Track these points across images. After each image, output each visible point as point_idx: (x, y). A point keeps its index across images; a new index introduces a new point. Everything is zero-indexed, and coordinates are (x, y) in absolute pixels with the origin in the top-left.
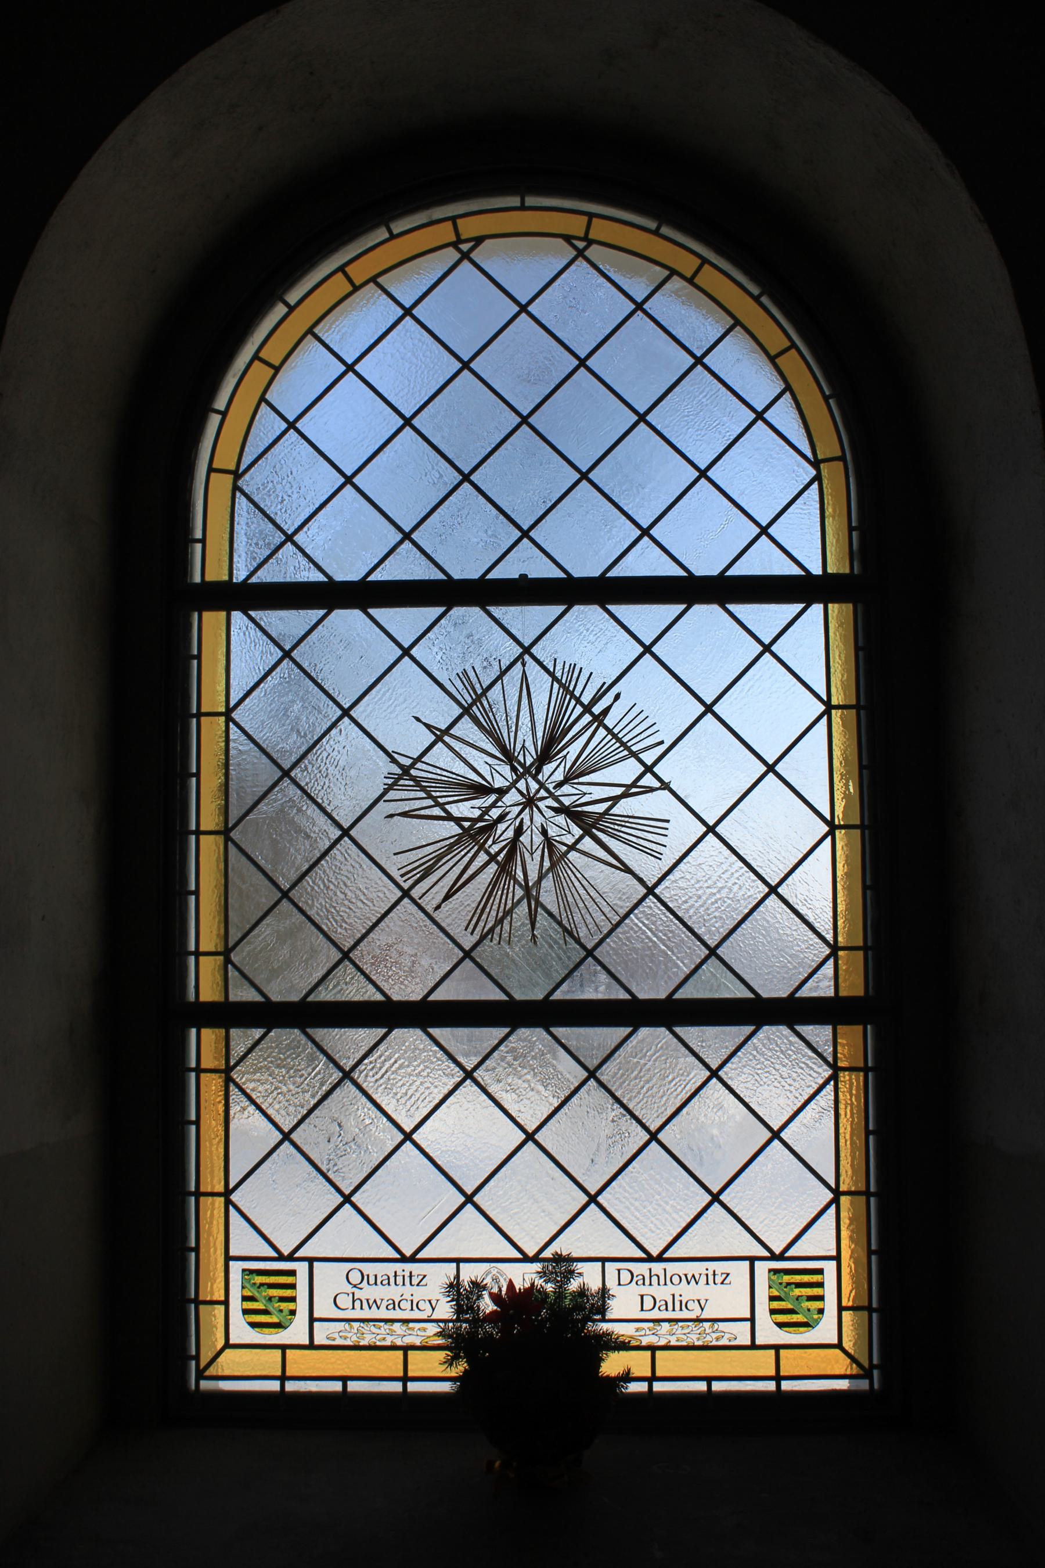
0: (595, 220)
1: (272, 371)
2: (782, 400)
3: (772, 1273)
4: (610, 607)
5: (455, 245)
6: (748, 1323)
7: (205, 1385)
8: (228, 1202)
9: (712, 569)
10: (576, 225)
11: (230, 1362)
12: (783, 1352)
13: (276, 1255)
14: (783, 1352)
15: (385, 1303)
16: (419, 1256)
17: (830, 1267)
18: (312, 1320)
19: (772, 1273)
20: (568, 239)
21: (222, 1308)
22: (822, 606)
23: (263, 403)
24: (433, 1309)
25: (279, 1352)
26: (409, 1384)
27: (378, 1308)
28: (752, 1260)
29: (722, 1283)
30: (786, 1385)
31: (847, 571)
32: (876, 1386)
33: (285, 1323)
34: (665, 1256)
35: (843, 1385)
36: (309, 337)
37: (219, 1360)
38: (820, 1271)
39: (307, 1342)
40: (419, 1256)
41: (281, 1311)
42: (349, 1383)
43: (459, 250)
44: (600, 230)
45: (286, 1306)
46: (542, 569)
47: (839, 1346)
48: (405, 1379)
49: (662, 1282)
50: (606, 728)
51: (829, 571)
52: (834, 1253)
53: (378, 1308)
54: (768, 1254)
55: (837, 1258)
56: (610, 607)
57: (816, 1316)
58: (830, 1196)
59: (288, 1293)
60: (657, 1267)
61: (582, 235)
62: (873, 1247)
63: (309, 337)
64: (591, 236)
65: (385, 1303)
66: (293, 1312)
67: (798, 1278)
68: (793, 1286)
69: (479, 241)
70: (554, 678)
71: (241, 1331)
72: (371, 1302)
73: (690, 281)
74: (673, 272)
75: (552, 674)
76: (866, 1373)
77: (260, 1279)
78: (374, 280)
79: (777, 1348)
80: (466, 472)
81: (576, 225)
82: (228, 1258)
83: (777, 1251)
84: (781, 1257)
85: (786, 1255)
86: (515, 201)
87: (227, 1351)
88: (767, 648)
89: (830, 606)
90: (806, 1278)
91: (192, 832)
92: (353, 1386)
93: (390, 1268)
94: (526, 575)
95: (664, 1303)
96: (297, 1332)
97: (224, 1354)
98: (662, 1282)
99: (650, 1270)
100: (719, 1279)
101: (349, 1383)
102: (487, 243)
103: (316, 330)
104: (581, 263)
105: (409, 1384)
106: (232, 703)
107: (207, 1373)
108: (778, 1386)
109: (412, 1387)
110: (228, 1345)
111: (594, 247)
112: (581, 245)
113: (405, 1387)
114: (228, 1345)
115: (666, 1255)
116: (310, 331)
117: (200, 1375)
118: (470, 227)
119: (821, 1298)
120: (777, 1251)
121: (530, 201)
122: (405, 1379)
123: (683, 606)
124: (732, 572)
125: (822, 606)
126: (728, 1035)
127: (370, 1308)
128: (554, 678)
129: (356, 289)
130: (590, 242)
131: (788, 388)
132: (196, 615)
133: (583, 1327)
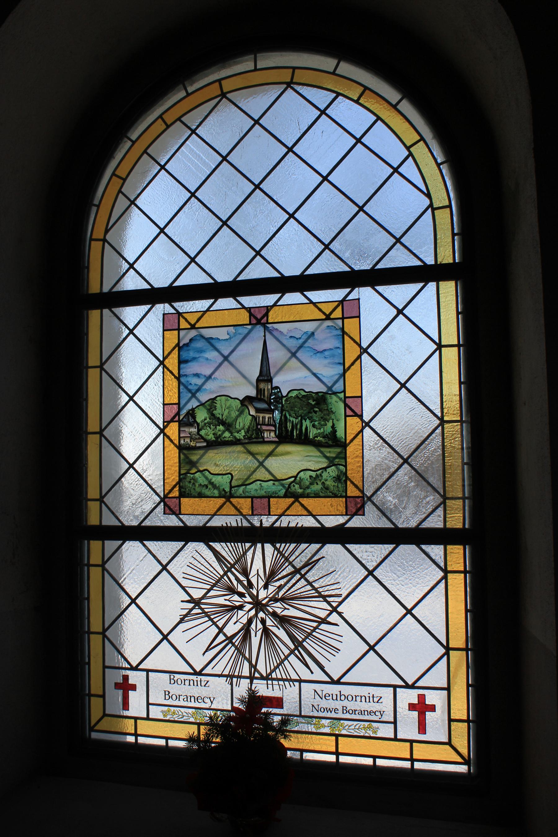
4: (319, 526)
6: (392, 725)
7: (94, 735)
8: (105, 636)
13: (193, 672)
23: (120, 194)
24: (212, 703)
25: (408, 744)
28: (395, 687)
29: (205, 686)
30: (343, 759)
39: (145, 716)
42: (169, 741)
49: (367, 700)
52: (446, 686)
56: (319, 526)
58: (443, 651)
72: (328, 709)
78: (179, 119)
80: (398, 237)
95: (186, 697)
97: (103, 720)
98: (367, 700)
100: (203, 684)
101: (169, 741)
107: (96, 728)
108: (412, 765)
115: (342, 681)
116: (145, 152)
117: (92, 729)
125: (435, 283)
129: (168, 126)
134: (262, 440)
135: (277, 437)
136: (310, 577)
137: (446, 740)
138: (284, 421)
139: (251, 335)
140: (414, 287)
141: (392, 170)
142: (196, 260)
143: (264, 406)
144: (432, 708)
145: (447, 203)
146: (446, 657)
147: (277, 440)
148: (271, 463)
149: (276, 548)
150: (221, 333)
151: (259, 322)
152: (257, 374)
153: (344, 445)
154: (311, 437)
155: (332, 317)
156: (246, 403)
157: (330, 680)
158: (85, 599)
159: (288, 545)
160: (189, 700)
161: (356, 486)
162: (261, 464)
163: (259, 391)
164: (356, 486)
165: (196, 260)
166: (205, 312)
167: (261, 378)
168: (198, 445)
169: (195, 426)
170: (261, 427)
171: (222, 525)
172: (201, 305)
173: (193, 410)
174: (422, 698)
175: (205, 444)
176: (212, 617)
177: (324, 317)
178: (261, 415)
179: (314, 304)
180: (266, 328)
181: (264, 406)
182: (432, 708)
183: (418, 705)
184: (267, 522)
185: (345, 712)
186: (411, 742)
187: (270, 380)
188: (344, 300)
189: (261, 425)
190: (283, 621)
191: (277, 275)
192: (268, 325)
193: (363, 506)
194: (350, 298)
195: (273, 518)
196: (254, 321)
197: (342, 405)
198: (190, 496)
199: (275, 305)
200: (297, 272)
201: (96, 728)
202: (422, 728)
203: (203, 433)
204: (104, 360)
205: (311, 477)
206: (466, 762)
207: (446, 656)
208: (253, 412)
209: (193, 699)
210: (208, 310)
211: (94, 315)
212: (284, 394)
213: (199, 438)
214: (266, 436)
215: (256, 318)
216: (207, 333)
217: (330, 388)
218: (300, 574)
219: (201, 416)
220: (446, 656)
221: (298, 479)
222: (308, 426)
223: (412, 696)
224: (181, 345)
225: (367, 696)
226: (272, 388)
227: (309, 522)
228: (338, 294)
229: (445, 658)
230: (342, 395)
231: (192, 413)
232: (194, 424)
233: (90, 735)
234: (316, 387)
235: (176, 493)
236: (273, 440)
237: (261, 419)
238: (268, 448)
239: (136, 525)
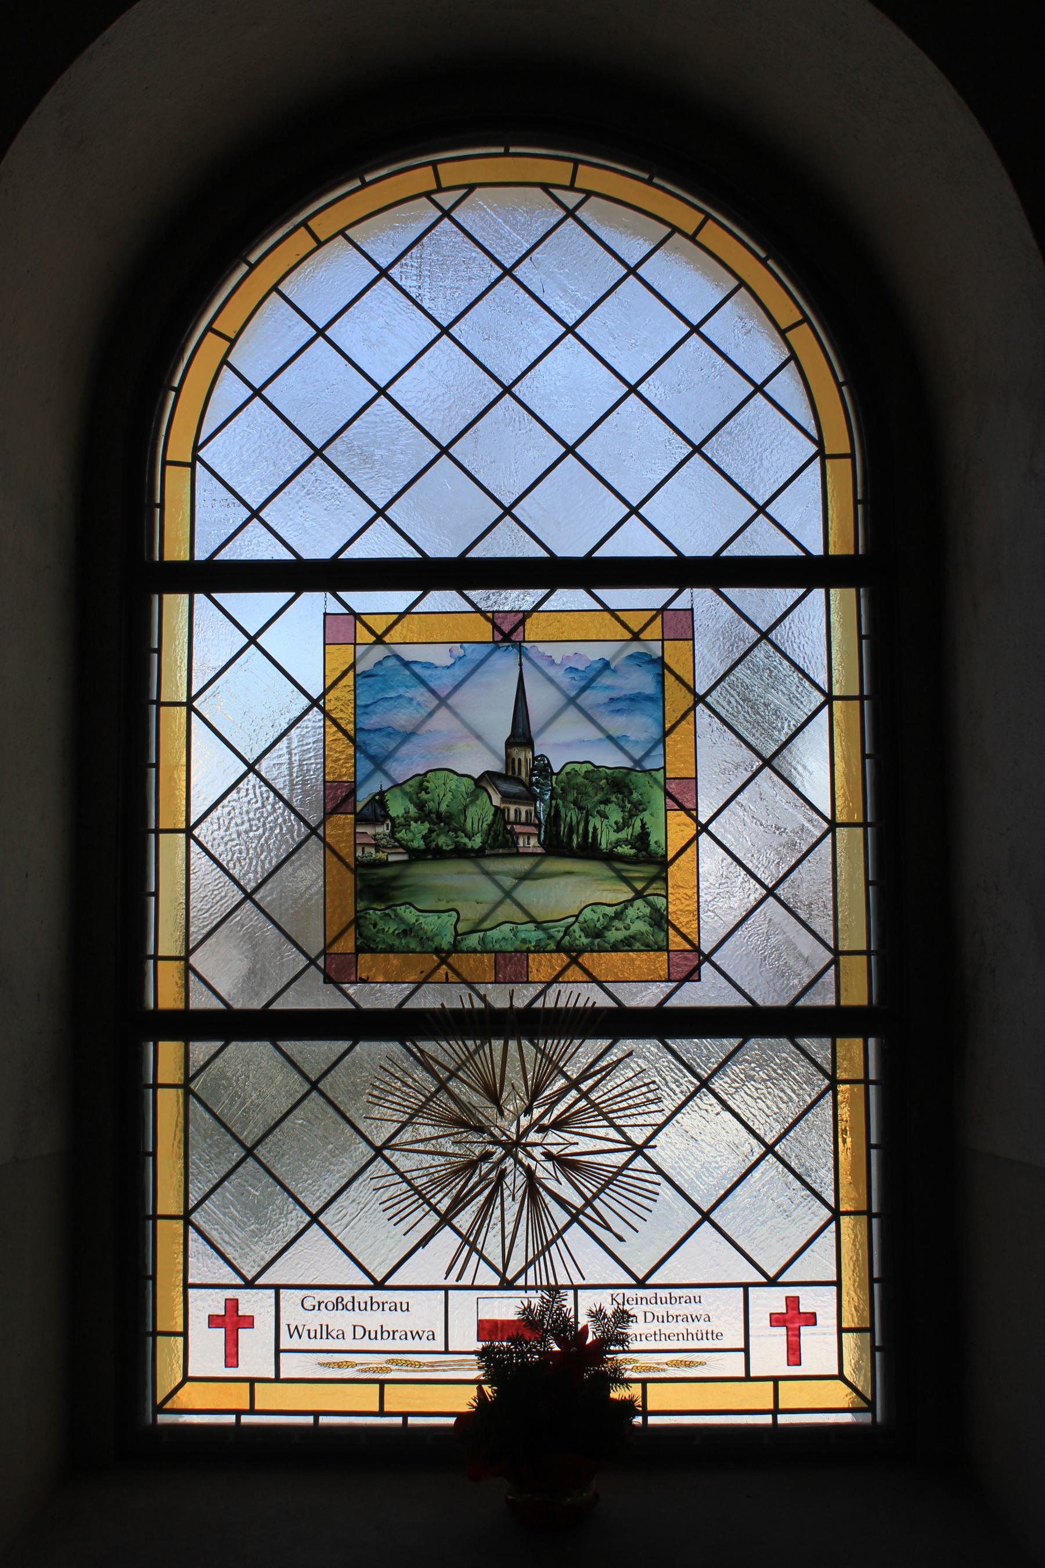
1: (228, 344)
4: (723, 590)
6: (742, 1354)
7: (163, 1419)
11: (190, 1396)
12: (782, 1384)
14: (782, 1384)
15: (426, 1335)
21: (180, 1340)
22: (822, 591)
26: (779, 1416)
27: (420, 1338)
28: (746, 1286)
31: (852, 552)
32: (879, 1419)
35: (847, 1418)
37: (179, 1393)
47: (841, 1377)
48: (775, 1411)
51: (831, 552)
53: (420, 1338)
60: (379, 1295)
62: (876, 1275)
65: (426, 1335)
73: (692, 238)
74: (675, 229)
76: (871, 1407)
87: (188, 1384)
89: (832, 591)
91: (152, 831)
92: (323, 1420)
93: (362, 1296)
99: (372, 1298)
103: (743, 290)
105: (779, 1416)
109: (782, 1419)
110: (186, 1379)
112: (570, 199)
113: (775, 1419)
114: (186, 1379)
122: (775, 1411)
123: (292, 594)
125: (822, 591)
126: (715, 1048)
127: (413, 1338)
132: (157, 597)
134: (515, 850)
135: (542, 845)
137: (836, 1372)
138: (554, 818)
139: (489, 662)
140: (789, 595)
141: (501, 511)
142: (633, 396)
143: (516, 789)
144: (811, 1319)
147: (540, 850)
148: (528, 894)
149: (536, 1046)
150: (440, 655)
151: (507, 637)
152: (508, 732)
153: (664, 863)
154: (604, 846)
155: (642, 636)
156: (484, 784)
158: (149, 1154)
159: (556, 1041)
160: (639, 1302)
161: (684, 937)
162: (508, 894)
163: (509, 761)
164: (684, 937)
165: (633, 396)
166: (402, 615)
167: (512, 740)
168: (391, 858)
169: (388, 825)
170: (512, 827)
171: (442, 1005)
172: (398, 600)
173: (382, 793)
174: (793, 1302)
175: (405, 857)
177: (629, 636)
178: (513, 808)
179: (612, 612)
180: (521, 651)
181: (516, 789)
182: (811, 1319)
183: (797, 1312)
184: (523, 997)
186: (776, 1380)
187: (529, 744)
188: (664, 608)
189: (513, 823)
191: (543, 554)
192: (523, 644)
193: (697, 969)
194: (673, 606)
195: (532, 990)
196: (499, 637)
197: (661, 794)
198: (372, 951)
199: (535, 609)
200: (580, 551)
201: (168, 1405)
202: (794, 1354)
203: (402, 835)
204: (194, 693)
205: (604, 915)
206: (871, 1407)
208: (497, 800)
209: (644, 1301)
210: (408, 611)
211: (176, 603)
212: (556, 770)
213: (395, 847)
214: (521, 844)
215: (319, 707)
216: (409, 653)
217: (638, 762)
218: (579, 1090)
219: (397, 807)
221: (581, 919)
222: (598, 826)
223: (773, 1300)
224: (359, 669)
226: (535, 759)
227: (595, 997)
228: (654, 597)
230: (660, 776)
231: (379, 801)
232: (385, 820)
233: (155, 1419)
234: (610, 759)
235: (347, 944)
236: (535, 851)
237: (512, 813)
238: (523, 865)
239: (259, 1007)
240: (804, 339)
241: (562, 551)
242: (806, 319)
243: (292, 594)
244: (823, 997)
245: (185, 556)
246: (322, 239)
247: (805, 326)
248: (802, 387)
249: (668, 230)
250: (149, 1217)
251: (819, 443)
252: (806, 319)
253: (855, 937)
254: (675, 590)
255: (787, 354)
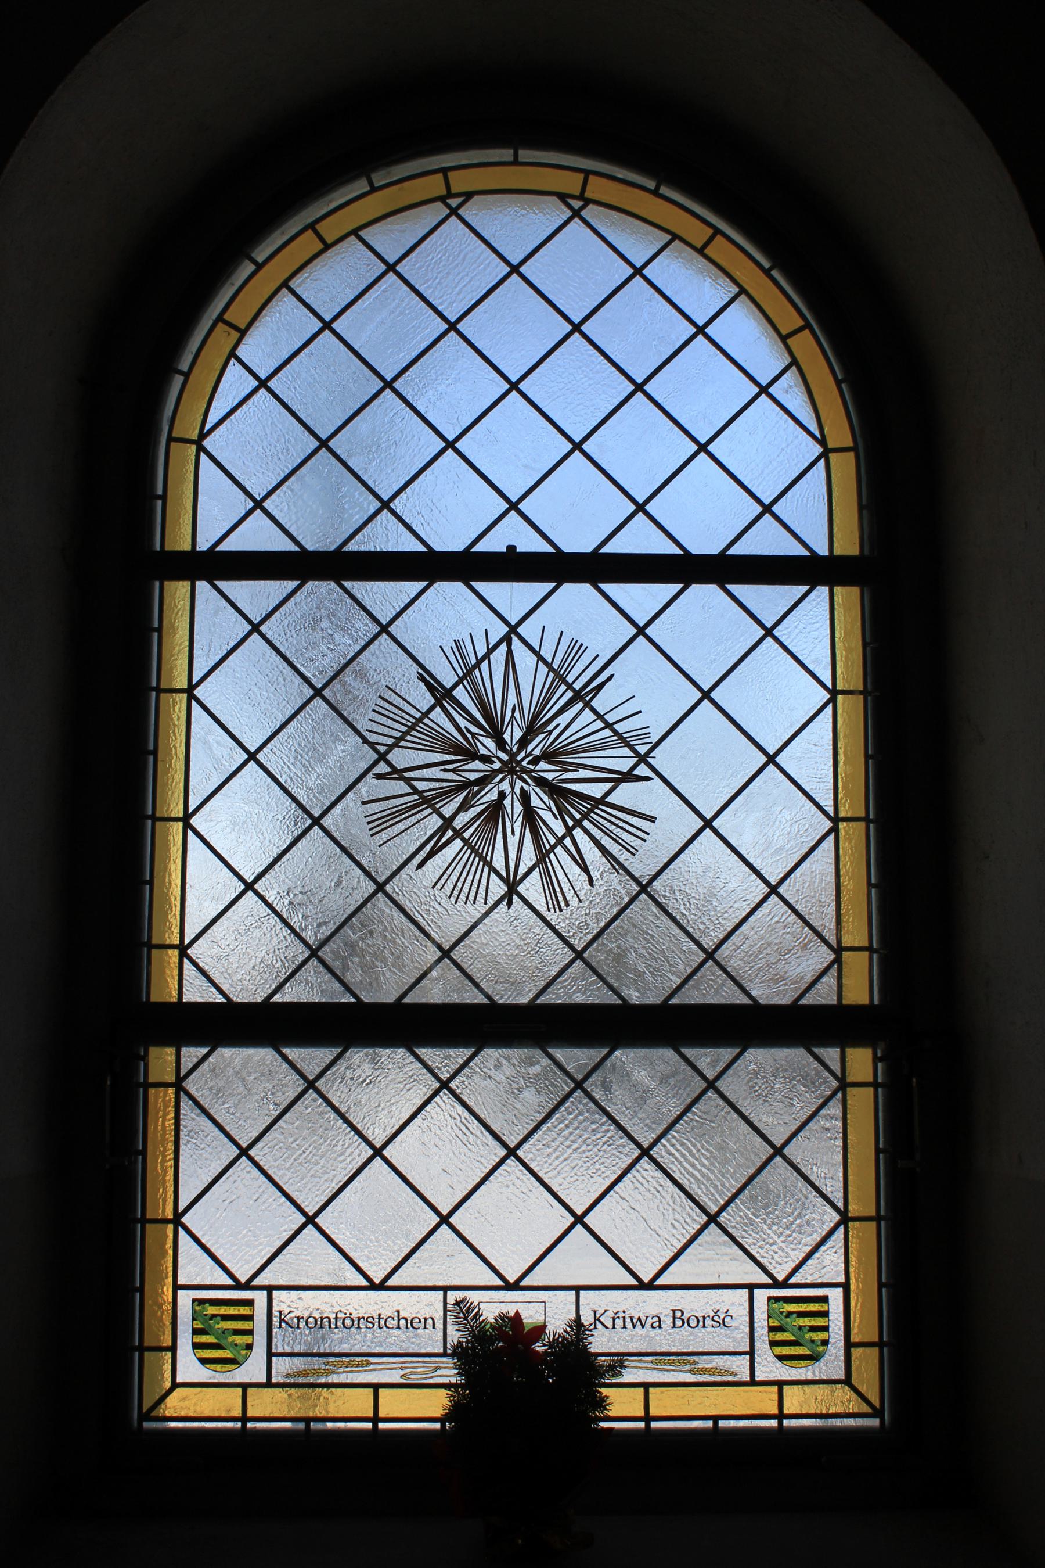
0: (591, 178)
2: (789, 373)
3: (196, 1303)
4: (601, 585)
5: (443, 199)
7: (147, 1425)
9: (455, 543)
10: (571, 183)
11: (176, 1404)
13: (367, 1284)
16: (659, 1282)
17: (836, 1296)
18: (270, 1354)
19: (196, 1303)
20: (563, 197)
28: (751, 1287)
33: (240, 1359)
34: (522, 1284)
36: (284, 291)
38: (825, 1299)
40: (658, 1282)
41: (813, 1341)
43: (448, 206)
44: (597, 188)
45: (240, 1340)
46: (530, 543)
47: (847, 1381)
50: (594, 710)
51: (835, 553)
54: (502, 1283)
55: (846, 1286)
56: (601, 585)
57: (244, 1352)
59: (820, 1322)
61: (577, 193)
63: (284, 291)
64: (588, 194)
66: (249, 1347)
67: (223, 1310)
68: (794, 1316)
69: (468, 196)
70: (540, 658)
71: (190, 1367)
75: (537, 654)
77: (212, 1310)
79: (780, 1384)
81: (571, 183)
82: (176, 1287)
83: (243, 1280)
84: (785, 1284)
85: (253, 1283)
86: (507, 154)
87: (854, 1382)
88: (769, 632)
90: (232, 1311)
94: (514, 547)
96: (253, 1369)
102: (476, 198)
104: (576, 224)
106: (195, 681)
111: (591, 206)
112: (577, 204)
114: (175, 1385)
118: (460, 182)
119: (825, 1329)
120: (243, 1280)
121: (525, 155)
123: (806, 588)
124: (733, 551)
128: (540, 658)
130: (588, 202)
131: (794, 362)
132: (157, 584)
133: (596, 1359)
136: (600, 703)
145: (710, 232)
146: (501, 1283)
157: (194, 683)
176: (548, 847)
185: (679, 1323)
190: (555, 791)
206: (877, 1413)
207: (636, 1283)
220: (636, 1283)
225: (332, 1316)
229: (634, 1282)
240: (805, 344)
241: (569, 546)
242: (807, 326)
243: (425, 583)
244: (824, 994)
245: (187, 547)
246: (329, 241)
247: (807, 332)
248: (637, 222)
249: (668, 237)
250: (138, 1221)
251: (822, 442)
252: (807, 326)
253: (856, 934)
254: (806, 588)
255: (787, 360)
